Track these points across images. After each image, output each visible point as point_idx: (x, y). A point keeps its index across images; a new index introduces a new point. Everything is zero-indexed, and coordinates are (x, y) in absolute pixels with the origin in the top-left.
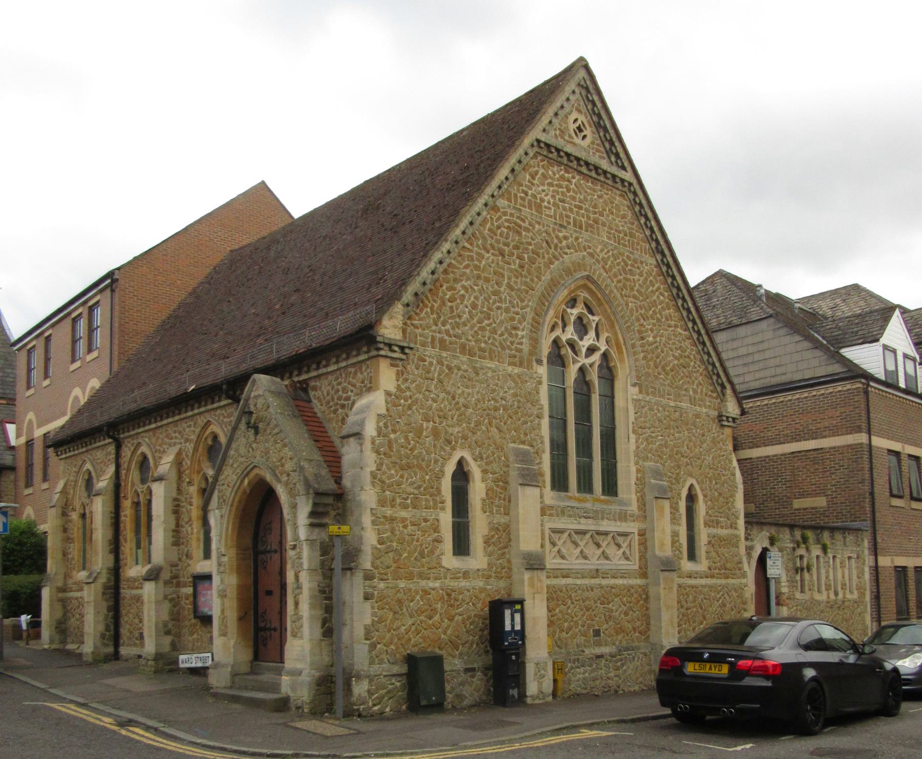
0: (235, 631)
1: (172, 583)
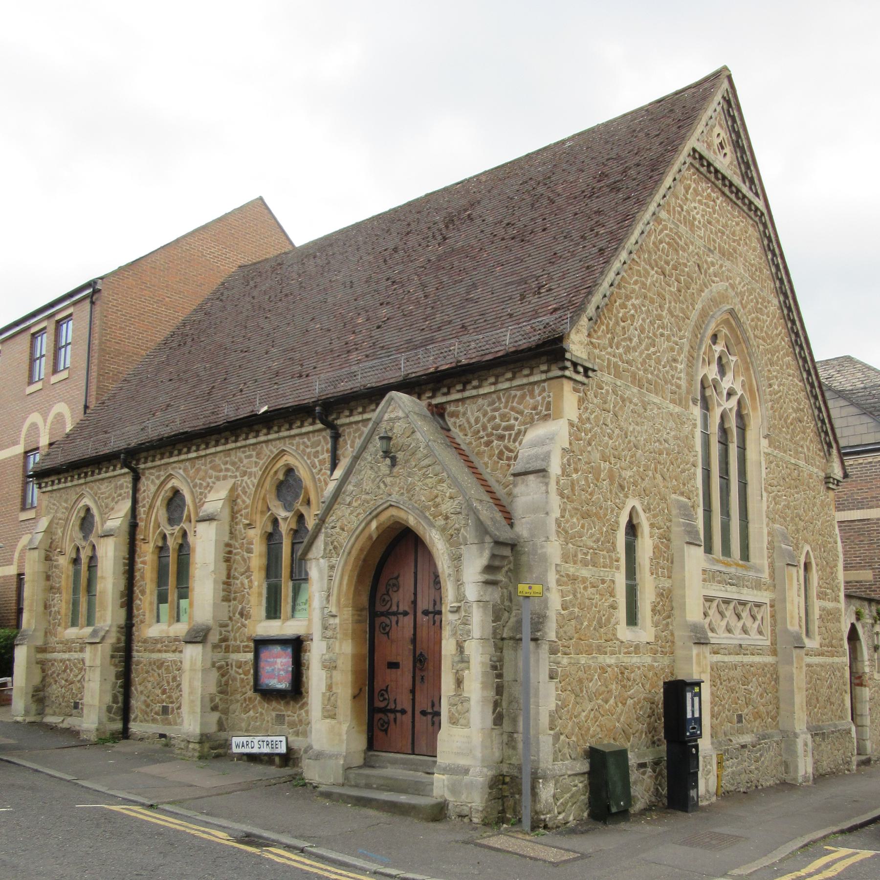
0: (349, 712)
1: (221, 647)
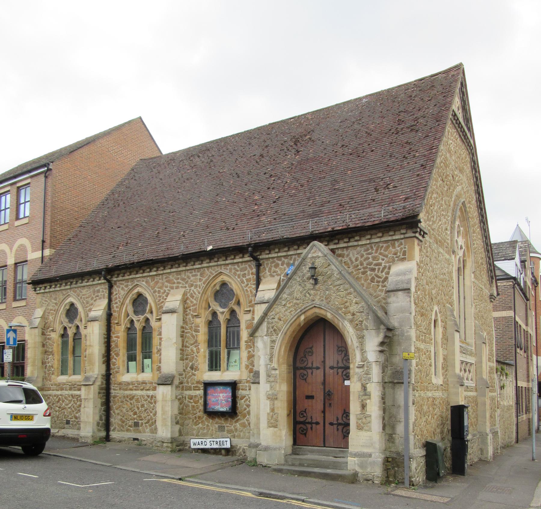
0: (286, 424)
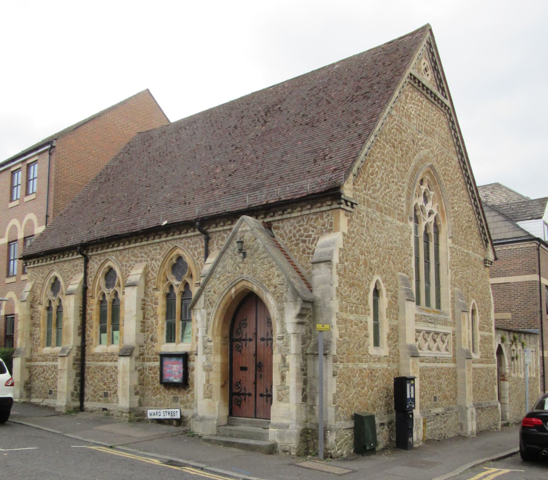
1: (140, 358)
